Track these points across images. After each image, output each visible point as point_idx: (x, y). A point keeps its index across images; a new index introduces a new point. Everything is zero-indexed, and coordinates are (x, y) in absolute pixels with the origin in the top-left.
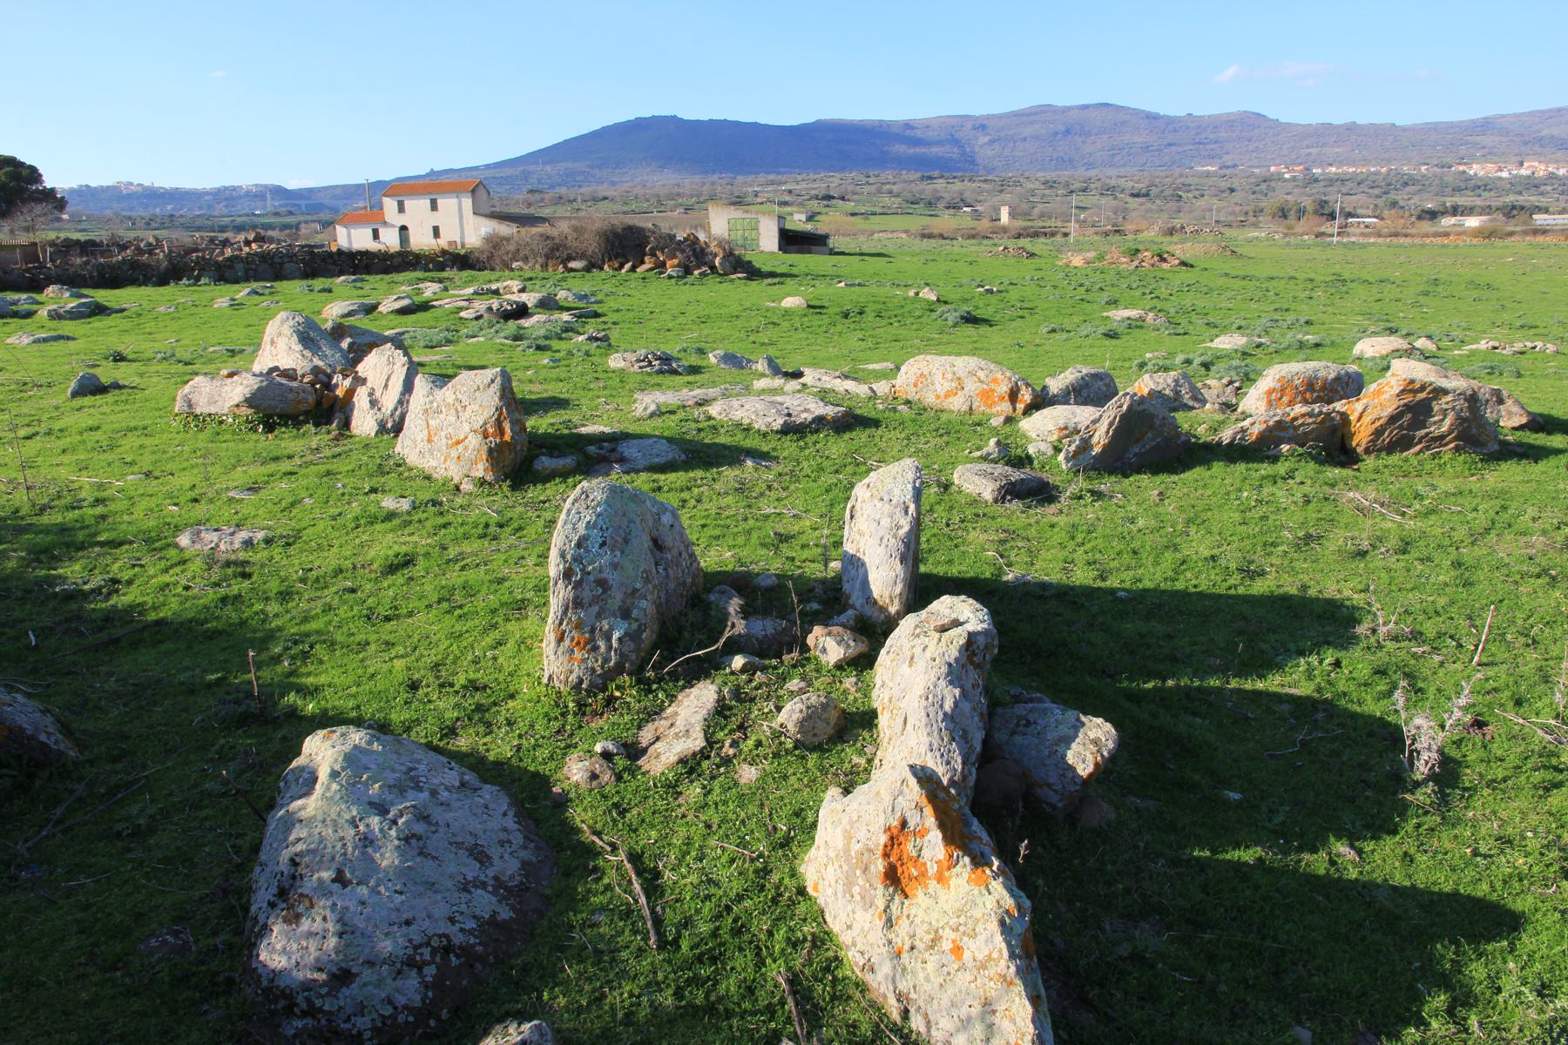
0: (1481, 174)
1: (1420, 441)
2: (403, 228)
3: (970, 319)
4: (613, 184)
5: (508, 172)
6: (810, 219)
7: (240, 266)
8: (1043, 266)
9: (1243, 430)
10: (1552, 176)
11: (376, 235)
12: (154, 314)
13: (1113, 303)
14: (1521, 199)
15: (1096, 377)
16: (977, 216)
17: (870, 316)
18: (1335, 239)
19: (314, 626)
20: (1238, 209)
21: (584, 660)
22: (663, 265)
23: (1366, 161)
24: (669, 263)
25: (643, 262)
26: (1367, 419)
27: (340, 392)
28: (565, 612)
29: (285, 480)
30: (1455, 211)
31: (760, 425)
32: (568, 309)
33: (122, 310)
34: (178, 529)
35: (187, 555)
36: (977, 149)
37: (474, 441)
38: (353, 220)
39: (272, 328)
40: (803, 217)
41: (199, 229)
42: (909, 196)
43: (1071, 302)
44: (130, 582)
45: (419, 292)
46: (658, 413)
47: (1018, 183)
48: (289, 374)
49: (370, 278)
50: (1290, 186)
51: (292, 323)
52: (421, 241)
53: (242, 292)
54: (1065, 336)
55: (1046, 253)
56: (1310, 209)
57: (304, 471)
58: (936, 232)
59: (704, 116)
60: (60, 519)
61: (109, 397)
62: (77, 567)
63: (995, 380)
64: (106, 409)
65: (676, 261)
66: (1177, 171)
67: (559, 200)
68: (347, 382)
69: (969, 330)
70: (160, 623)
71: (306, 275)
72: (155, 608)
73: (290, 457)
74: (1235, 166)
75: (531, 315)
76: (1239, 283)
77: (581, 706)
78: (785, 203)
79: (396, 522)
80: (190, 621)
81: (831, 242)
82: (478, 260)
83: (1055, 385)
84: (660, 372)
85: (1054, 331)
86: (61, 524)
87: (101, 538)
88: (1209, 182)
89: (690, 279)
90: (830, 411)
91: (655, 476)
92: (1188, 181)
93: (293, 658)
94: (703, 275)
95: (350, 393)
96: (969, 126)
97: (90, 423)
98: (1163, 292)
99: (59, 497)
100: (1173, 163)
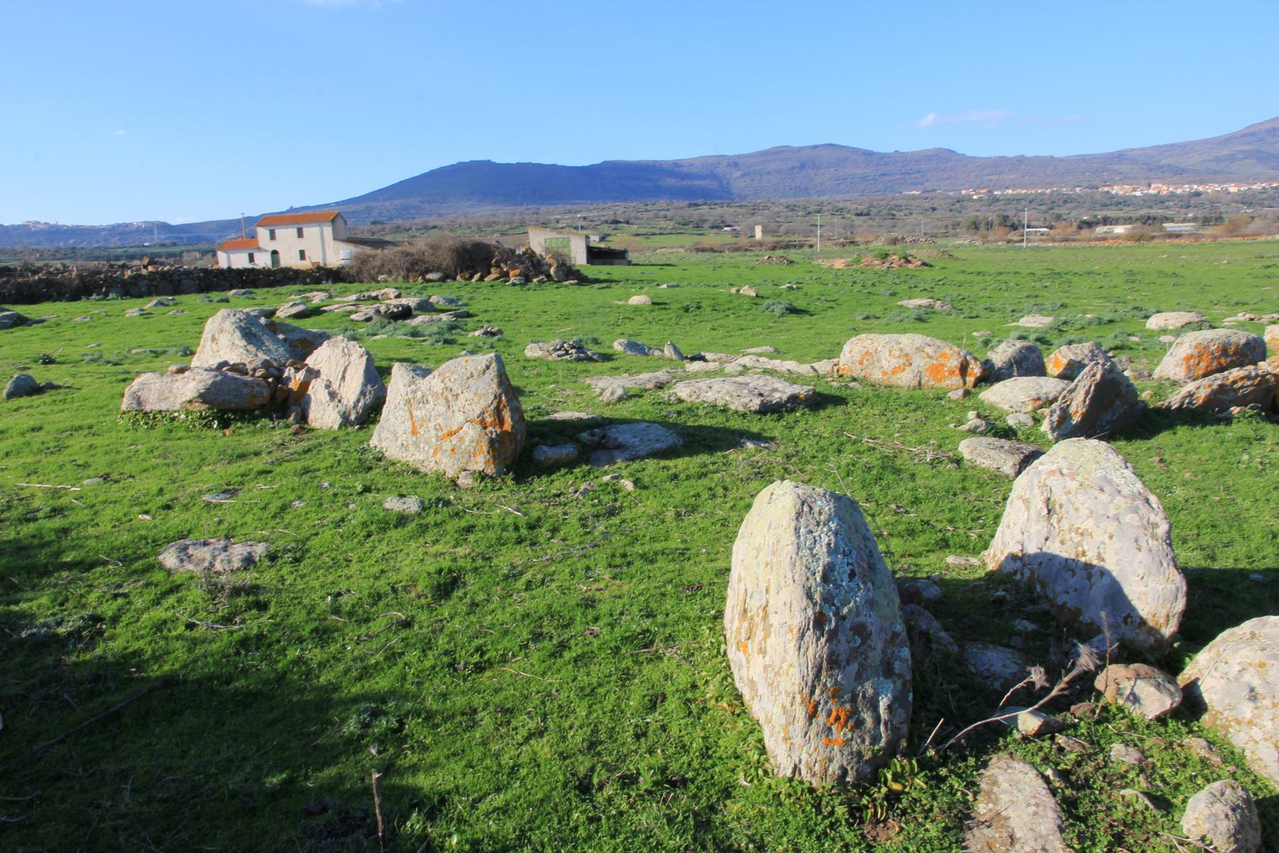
0: (1121, 193)
2: (275, 253)
3: (793, 310)
4: (440, 215)
5: (354, 207)
7: (143, 283)
9: (1190, 395)
10: (1172, 195)
11: (251, 258)
12: (71, 324)
14: (1153, 212)
16: (736, 234)
18: (1024, 244)
19: (382, 683)
20: (939, 223)
21: (847, 742)
22: (506, 275)
23: (1034, 185)
24: (511, 273)
25: (489, 273)
27: (293, 385)
28: (817, 676)
29: (262, 479)
30: (1106, 221)
31: (736, 405)
32: (443, 311)
33: (43, 321)
34: (158, 544)
35: (177, 578)
37: (471, 432)
38: (230, 247)
39: (211, 326)
40: (597, 238)
41: (97, 258)
42: (682, 221)
44: (115, 620)
45: (308, 300)
46: (627, 397)
47: (765, 208)
48: (239, 368)
49: (258, 291)
50: (978, 206)
51: (233, 319)
52: (289, 260)
53: (150, 304)
56: (996, 222)
57: (278, 469)
58: (707, 246)
60: (12, 536)
61: (47, 397)
62: (44, 600)
63: (943, 355)
64: (43, 409)
65: (517, 271)
67: (397, 229)
68: (301, 376)
69: (793, 319)
70: (169, 681)
71: (201, 290)
72: (156, 658)
73: (257, 454)
74: (934, 190)
75: (416, 316)
77: (856, 813)
79: (411, 527)
80: (210, 678)
81: (632, 256)
82: (348, 274)
84: (579, 360)
85: (867, 318)
86: (16, 541)
87: (68, 558)
88: (916, 203)
89: (530, 285)
90: (801, 390)
91: (663, 463)
92: (900, 202)
93: (381, 740)
94: (541, 282)
95: (305, 385)
96: (725, 163)
97: (31, 423)
99: (9, 508)
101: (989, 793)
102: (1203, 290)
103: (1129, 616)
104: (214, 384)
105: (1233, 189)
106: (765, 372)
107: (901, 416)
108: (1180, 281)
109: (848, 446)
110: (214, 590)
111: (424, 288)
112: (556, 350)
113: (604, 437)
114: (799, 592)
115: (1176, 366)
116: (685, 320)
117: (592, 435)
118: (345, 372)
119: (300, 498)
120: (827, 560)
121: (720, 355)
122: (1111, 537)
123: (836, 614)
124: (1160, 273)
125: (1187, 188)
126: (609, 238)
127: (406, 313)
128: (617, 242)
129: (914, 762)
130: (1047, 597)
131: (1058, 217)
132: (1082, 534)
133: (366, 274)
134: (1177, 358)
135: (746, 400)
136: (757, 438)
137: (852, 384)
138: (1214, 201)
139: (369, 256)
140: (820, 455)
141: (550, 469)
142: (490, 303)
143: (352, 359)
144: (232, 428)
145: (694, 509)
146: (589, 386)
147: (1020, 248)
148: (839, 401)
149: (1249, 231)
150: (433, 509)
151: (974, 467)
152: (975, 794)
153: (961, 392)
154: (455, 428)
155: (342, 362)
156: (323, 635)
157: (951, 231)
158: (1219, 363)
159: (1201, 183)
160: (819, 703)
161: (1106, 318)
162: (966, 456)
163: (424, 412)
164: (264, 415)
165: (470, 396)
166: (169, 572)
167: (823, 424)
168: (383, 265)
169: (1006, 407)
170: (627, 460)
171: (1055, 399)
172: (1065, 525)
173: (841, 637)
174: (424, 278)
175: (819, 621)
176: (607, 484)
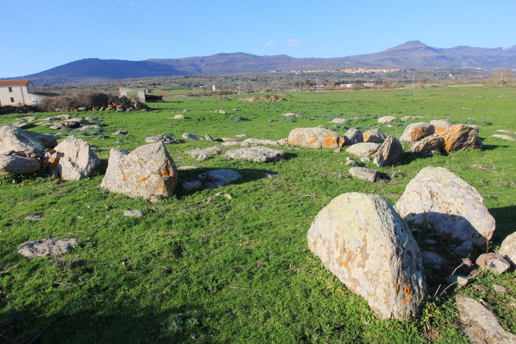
3: (243, 119)
4: (76, 82)
9: (418, 147)
10: (365, 73)
14: (359, 79)
16: (205, 89)
18: (317, 91)
22: (115, 107)
23: (317, 69)
24: (117, 107)
25: (107, 107)
26: (450, 140)
28: (398, 274)
30: (344, 82)
37: (155, 178)
45: (25, 121)
46: (208, 158)
47: (216, 78)
50: (297, 77)
51: (11, 130)
56: (305, 83)
58: (194, 94)
59: (108, 58)
63: (330, 135)
65: (120, 106)
67: (56, 88)
68: (54, 156)
69: (244, 123)
70: (60, 317)
73: (44, 194)
75: (82, 127)
79: (142, 224)
81: (164, 99)
82: (41, 108)
84: (171, 143)
85: (272, 121)
88: (274, 76)
90: (281, 152)
91: (238, 186)
94: (131, 110)
95: (57, 160)
96: (198, 60)
101: (463, 312)
103: (474, 234)
104: (11, 162)
105: (385, 71)
106: (258, 145)
107: (321, 160)
109: (307, 174)
110: (61, 266)
111: (79, 114)
112: (160, 139)
113: (208, 176)
114: (389, 240)
116: (200, 125)
117: (203, 175)
118: (78, 153)
119: (79, 214)
120: (394, 225)
121: (228, 138)
122: (462, 204)
123: (402, 247)
126: (152, 91)
127: (77, 125)
128: (156, 92)
129: (434, 303)
130: (434, 230)
131: (327, 81)
132: (449, 204)
133: (49, 108)
135: (260, 157)
136: (270, 172)
137: (295, 148)
138: (379, 76)
139: (50, 100)
140: (298, 178)
141: (191, 192)
142: (113, 120)
143: (81, 147)
144: (23, 182)
145: (261, 205)
146: (188, 154)
147: (315, 93)
148: (295, 156)
149: (392, 86)
150: (148, 215)
151: (357, 179)
152: (458, 313)
153: (339, 150)
154: (146, 177)
155: (75, 148)
156: (131, 282)
157: (289, 87)
159: (374, 69)
160: (400, 285)
161: (364, 119)
162: (353, 175)
163: (129, 170)
164: (39, 175)
165: (153, 161)
166: (28, 259)
167: (292, 165)
168: (57, 104)
169: (359, 155)
170: (223, 185)
171: (376, 151)
172: (440, 201)
173: (405, 257)
174: (77, 110)
175: (398, 251)
176: (219, 197)
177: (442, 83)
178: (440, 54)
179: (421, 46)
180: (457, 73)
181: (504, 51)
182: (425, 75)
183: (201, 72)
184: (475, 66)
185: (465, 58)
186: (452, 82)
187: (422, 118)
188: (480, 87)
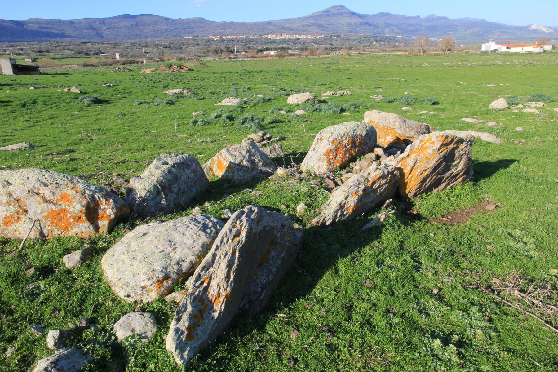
1: (445, 181)
6: (34, 60)
8: (134, 74)
9: (342, 207)
10: (290, 39)
13: (167, 87)
14: (284, 46)
15: (182, 165)
16: (106, 57)
17: (39, 104)
18: (236, 59)
20: (201, 51)
23: (238, 34)
26: (417, 172)
30: (267, 49)
36: (103, 31)
40: (30, 60)
42: (77, 50)
43: (148, 88)
47: (121, 44)
54: (147, 105)
55: (135, 70)
56: (224, 50)
58: (90, 64)
63: (64, 197)
66: (179, 38)
69: (97, 107)
74: (198, 36)
76: (213, 75)
78: (21, 54)
81: (41, 70)
83: (142, 185)
85: (141, 103)
88: (190, 42)
92: (184, 41)
96: (98, 22)
98: (187, 82)
100: (177, 35)
102: (307, 78)
105: (310, 37)
108: (298, 74)
115: (319, 160)
124: (290, 71)
125: (294, 37)
126: (38, 60)
131: (249, 48)
134: (319, 153)
147: (234, 61)
157: (206, 54)
158: (351, 154)
159: (299, 35)
177: (366, 50)
178: (364, 20)
179: (346, 11)
180: (380, 41)
181: (421, 20)
182: (351, 42)
183: (102, 37)
184: (397, 33)
185: (387, 25)
186: (377, 50)
187: (349, 93)
188: (403, 55)
